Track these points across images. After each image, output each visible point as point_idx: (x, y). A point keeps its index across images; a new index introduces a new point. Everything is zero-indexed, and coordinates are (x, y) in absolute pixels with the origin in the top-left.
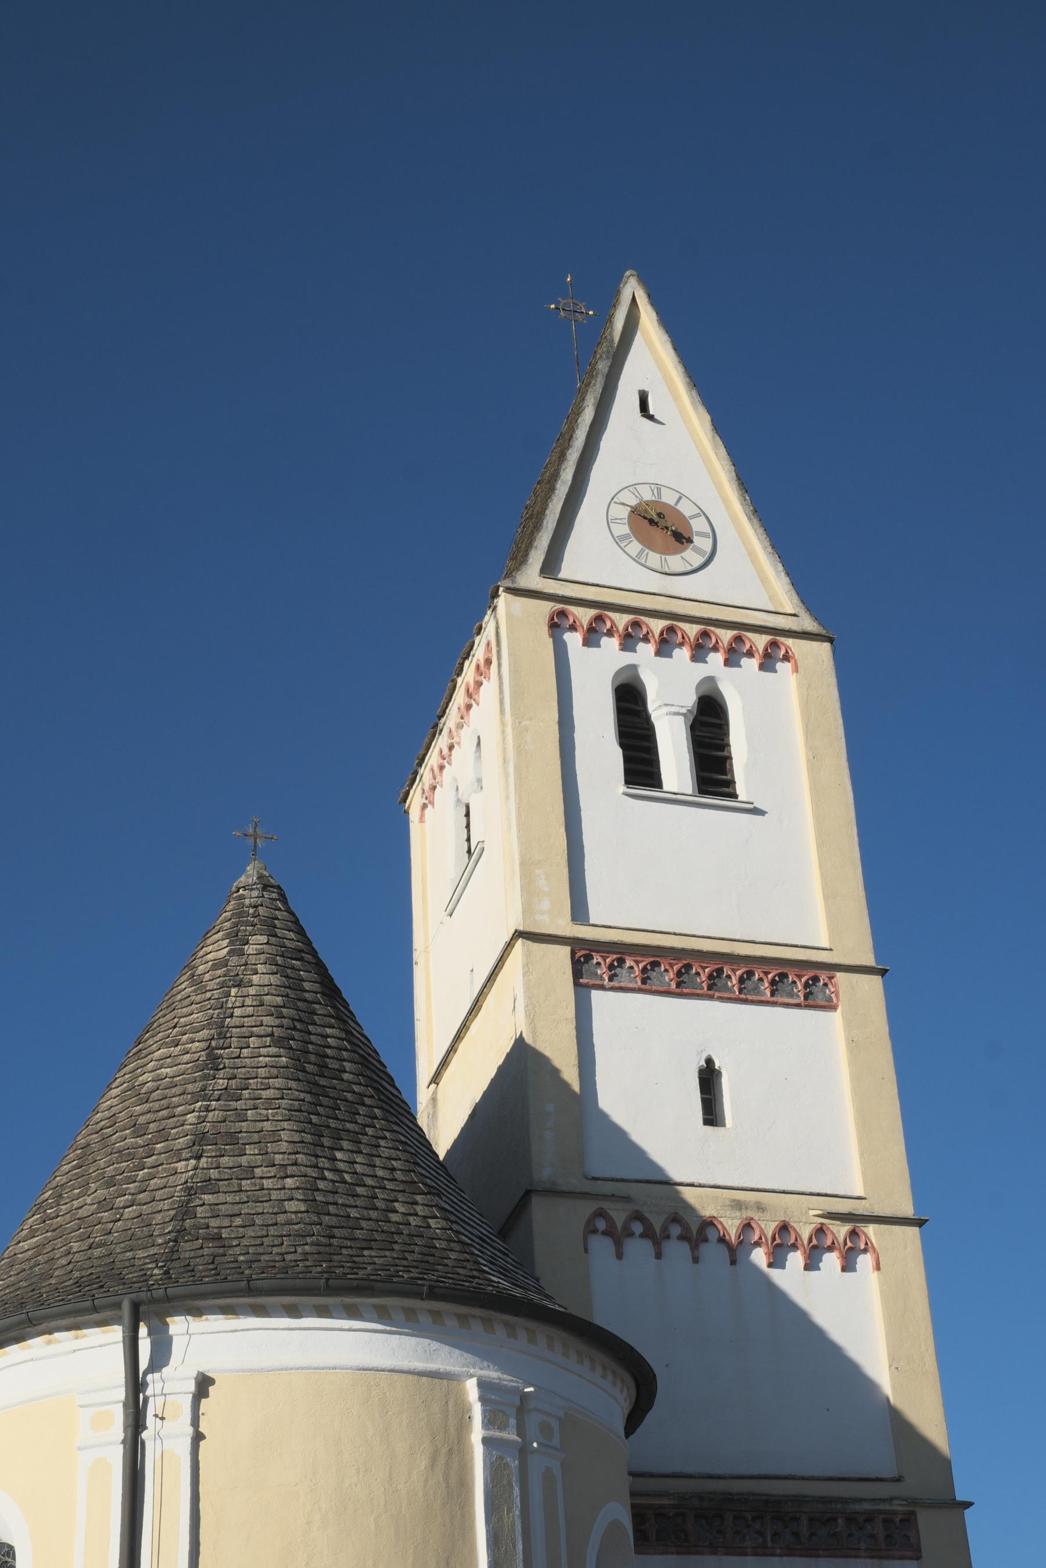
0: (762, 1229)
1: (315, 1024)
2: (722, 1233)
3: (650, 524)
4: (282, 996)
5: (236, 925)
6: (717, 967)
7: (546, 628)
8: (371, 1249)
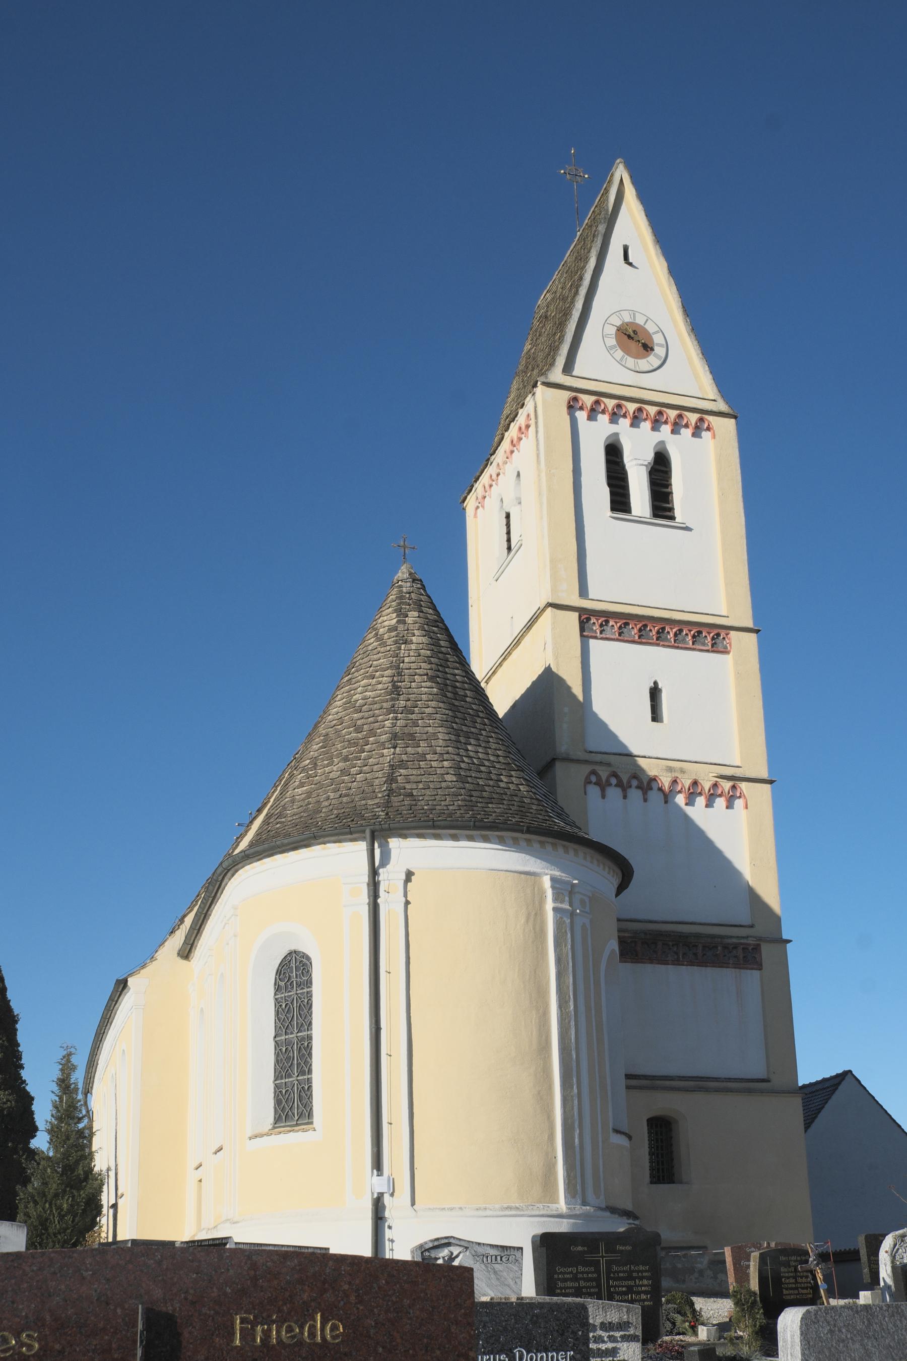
1: (448, 667)
2: (660, 786)
3: (629, 338)
4: (430, 650)
5: (399, 604)
6: (662, 626)
8: (492, 803)
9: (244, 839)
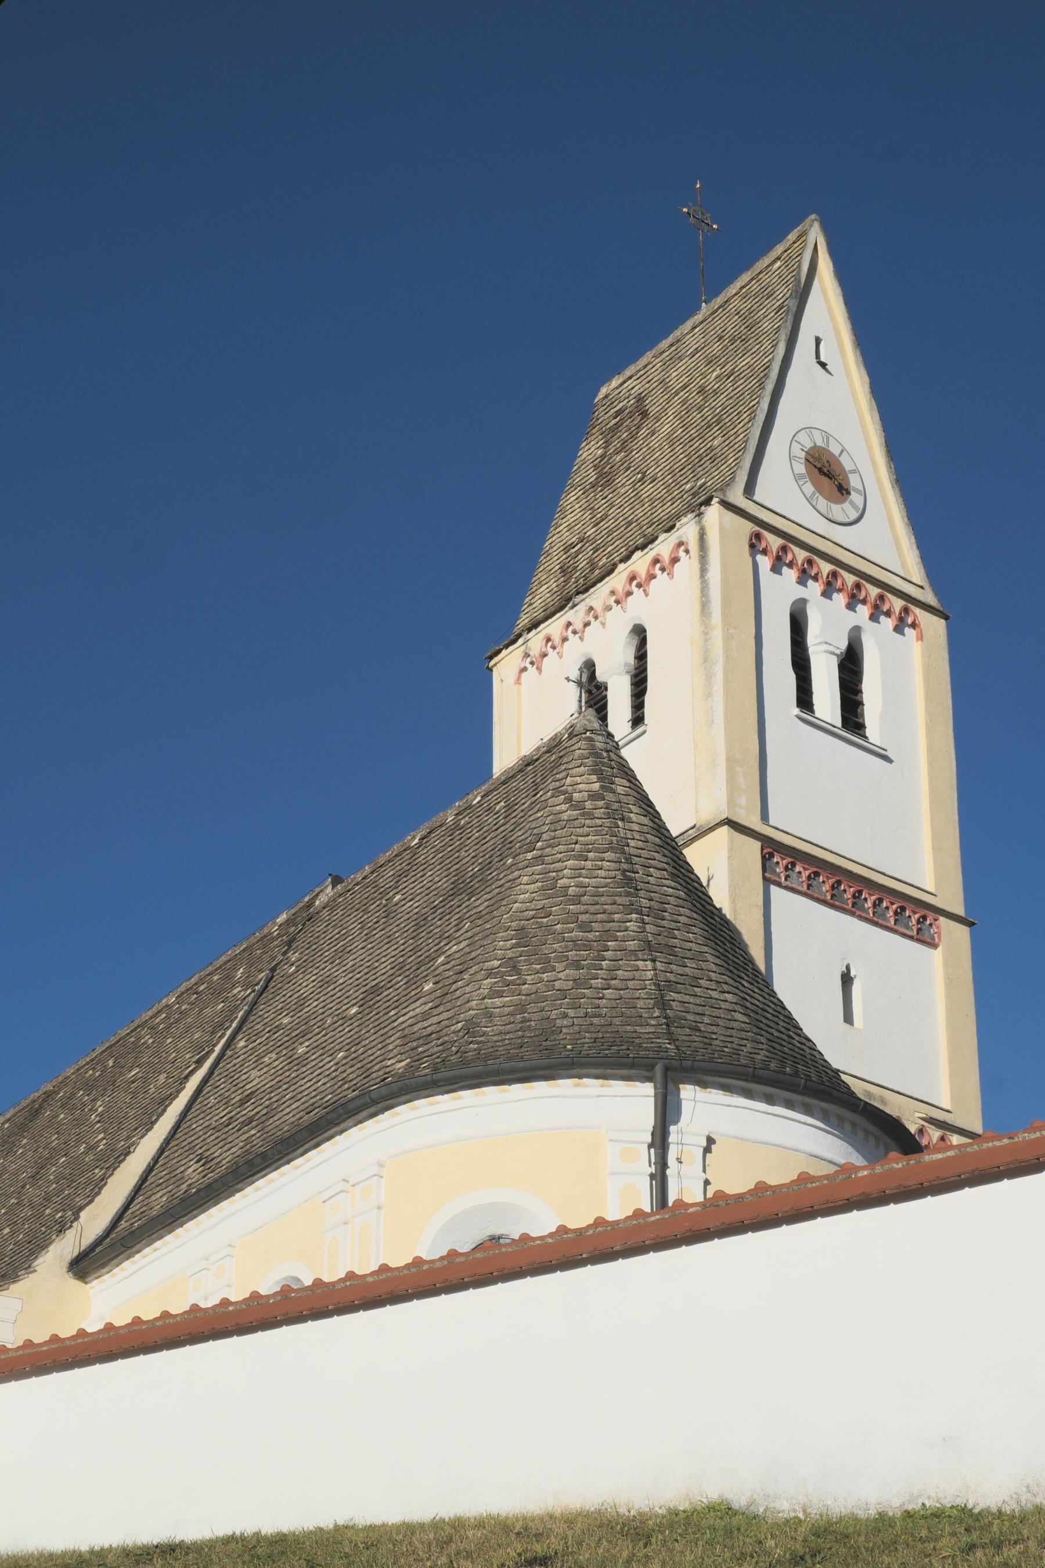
3: (820, 473)
9: (174, 1102)
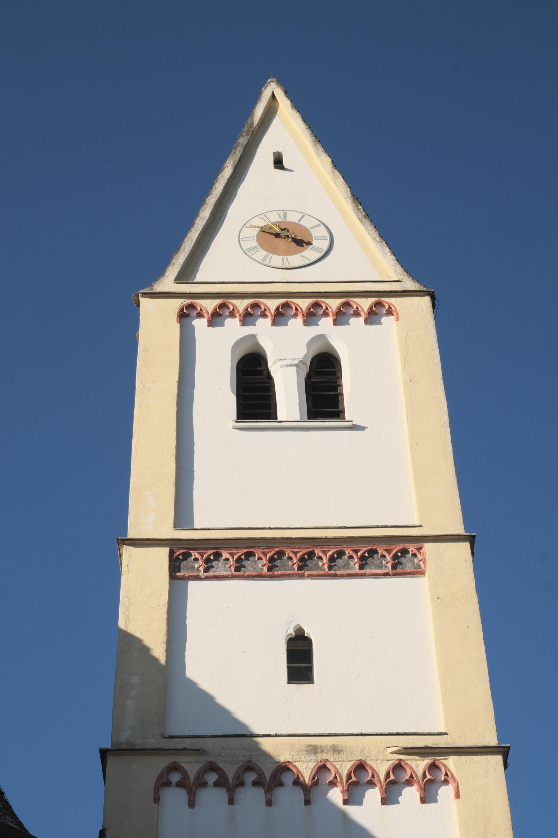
0: (337, 769)
2: (296, 776)
6: (308, 550)
7: (176, 317)
